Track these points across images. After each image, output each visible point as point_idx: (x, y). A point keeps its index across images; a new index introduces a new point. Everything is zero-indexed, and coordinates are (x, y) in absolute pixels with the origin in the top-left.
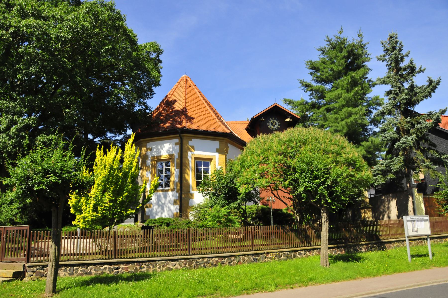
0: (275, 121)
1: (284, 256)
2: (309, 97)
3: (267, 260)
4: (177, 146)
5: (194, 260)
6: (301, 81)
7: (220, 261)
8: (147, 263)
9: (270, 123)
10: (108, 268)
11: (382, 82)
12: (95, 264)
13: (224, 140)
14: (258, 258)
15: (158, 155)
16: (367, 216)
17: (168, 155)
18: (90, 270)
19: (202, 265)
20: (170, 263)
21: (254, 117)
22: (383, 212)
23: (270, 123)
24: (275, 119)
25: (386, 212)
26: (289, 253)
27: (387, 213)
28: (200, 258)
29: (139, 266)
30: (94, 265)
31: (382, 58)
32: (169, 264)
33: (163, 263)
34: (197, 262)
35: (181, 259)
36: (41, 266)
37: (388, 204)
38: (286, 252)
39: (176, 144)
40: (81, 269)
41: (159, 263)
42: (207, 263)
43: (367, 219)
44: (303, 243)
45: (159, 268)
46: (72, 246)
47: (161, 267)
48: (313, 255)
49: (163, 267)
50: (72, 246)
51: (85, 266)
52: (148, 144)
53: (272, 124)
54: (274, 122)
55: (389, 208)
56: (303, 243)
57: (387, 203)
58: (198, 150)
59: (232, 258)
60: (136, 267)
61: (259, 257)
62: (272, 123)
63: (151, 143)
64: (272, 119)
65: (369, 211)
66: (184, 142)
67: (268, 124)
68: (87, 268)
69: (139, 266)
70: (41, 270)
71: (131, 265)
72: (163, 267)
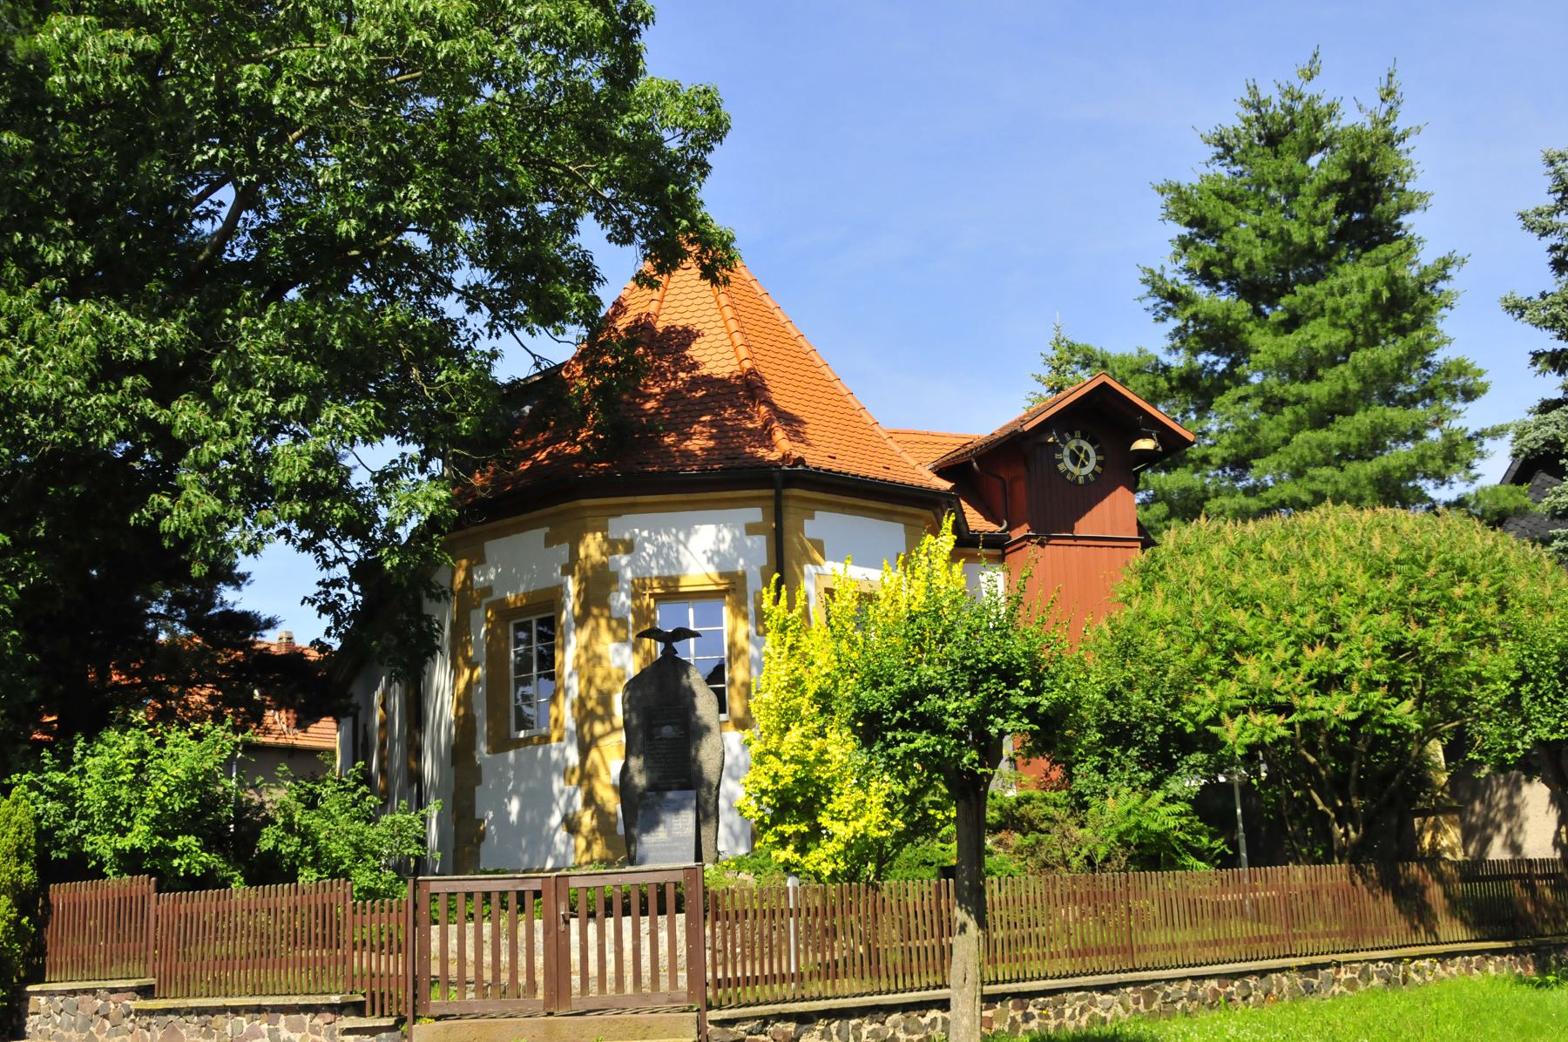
0: (1086, 446)
1: (1380, 974)
2: (1169, 343)
3: (1336, 989)
4: (756, 538)
5: (1158, 988)
6: (1152, 272)
7: (1221, 990)
8: (1041, 1000)
9: (1066, 452)
10: (940, 1021)
11: (1545, 320)
12: (905, 1008)
13: (918, 517)
14: (1316, 982)
15: (666, 573)
16: (1445, 843)
17: (715, 577)
18: (891, 1032)
19: (1179, 1006)
20: (1098, 996)
21: (1027, 428)
22: (1484, 827)
23: (1066, 452)
24: (1083, 438)
25: (1498, 828)
26: (1391, 966)
27: (1504, 830)
28: (1173, 980)
29: (1020, 1012)
30: (903, 1012)
31: (1545, 220)
32: (1093, 1003)
33: (1079, 998)
34: (1167, 995)
35: (1125, 985)
36: (760, 1017)
37: (1510, 797)
38: (1385, 960)
39: (751, 529)
40: (870, 1028)
41: (1070, 997)
42: (1192, 997)
43: (1448, 855)
44: (1416, 929)
45: (1072, 1017)
46: (610, 957)
47: (1077, 1012)
48: (1451, 974)
49: (1081, 1014)
50: (610, 957)
51: (881, 1014)
52: (612, 522)
53: (1075, 459)
54: (1080, 449)
55: (1512, 811)
56: (1416, 929)
57: (1503, 792)
58: (839, 558)
59: (1252, 982)
60: (1012, 1013)
61: (1317, 978)
62: (1072, 452)
63: (627, 519)
64: (1073, 436)
65: (1453, 823)
66: (789, 521)
67: (1057, 456)
68: (883, 1023)
69: (1020, 1012)
70: (761, 1033)
71: (998, 1006)
72: (1081, 1014)
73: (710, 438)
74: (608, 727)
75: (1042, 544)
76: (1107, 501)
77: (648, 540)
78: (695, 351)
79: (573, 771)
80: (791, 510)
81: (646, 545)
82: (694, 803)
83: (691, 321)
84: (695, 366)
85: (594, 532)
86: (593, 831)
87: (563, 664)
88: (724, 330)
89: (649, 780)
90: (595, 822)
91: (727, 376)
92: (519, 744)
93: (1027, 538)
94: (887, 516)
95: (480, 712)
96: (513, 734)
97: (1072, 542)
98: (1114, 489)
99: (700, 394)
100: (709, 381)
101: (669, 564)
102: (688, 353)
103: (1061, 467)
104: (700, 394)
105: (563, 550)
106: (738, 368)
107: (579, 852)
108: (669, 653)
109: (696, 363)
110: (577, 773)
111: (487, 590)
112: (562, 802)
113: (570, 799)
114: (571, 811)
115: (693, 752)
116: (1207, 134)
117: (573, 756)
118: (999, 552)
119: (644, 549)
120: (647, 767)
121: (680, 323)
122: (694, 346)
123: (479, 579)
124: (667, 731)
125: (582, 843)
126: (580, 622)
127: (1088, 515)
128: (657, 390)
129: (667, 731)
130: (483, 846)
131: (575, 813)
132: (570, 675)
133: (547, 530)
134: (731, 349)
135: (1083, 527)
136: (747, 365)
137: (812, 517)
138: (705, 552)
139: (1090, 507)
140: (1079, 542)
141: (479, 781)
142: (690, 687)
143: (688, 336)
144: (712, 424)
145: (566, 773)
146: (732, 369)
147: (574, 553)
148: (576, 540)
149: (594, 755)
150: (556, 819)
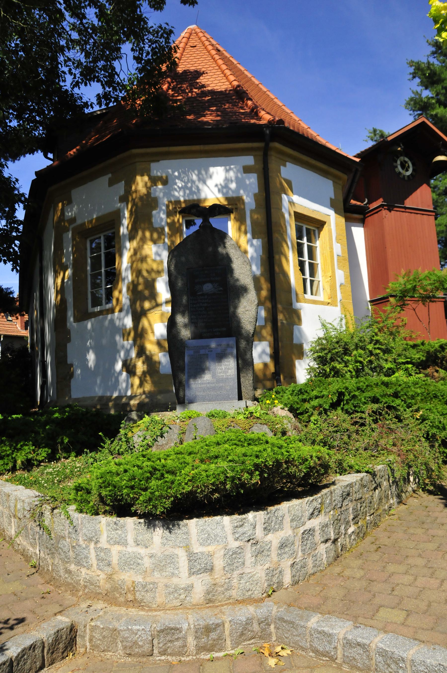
4: (251, 175)
9: (399, 162)
23: (399, 162)
39: (247, 170)
52: (153, 165)
53: (403, 165)
63: (164, 163)
73: (218, 116)
74: (154, 303)
75: (390, 211)
76: (418, 191)
77: (179, 178)
78: (202, 80)
79: (129, 334)
80: (273, 158)
81: (177, 181)
82: (235, 352)
83: (198, 67)
84: (203, 86)
85: (142, 175)
86: (144, 373)
87: (121, 263)
88: (219, 70)
89: (192, 333)
90: (145, 367)
91: (224, 90)
92: (95, 315)
93: (382, 206)
94: (324, 174)
95: (70, 300)
96: (90, 310)
97: (403, 210)
98: (421, 185)
99: (207, 98)
100: (213, 93)
101: (192, 193)
102: (198, 81)
103: (397, 170)
104: (207, 98)
105: (120, 188)
106: (230, 86)
107: (135, 387)
108: (206, 226)
109: (204, 85)
110: (132, 334)
111: (73, 220)
112: (122, 354)
113: (128, 352)
114: (129, 358)
115: (232, 309)
116: (430, 41)
117: (128, 322)
118: (361, 216)
119: (176, 184)
120: (193, 322)
121: (192, 68)
122: (201, 78)
123: (69, 214)
124: (208, 287)
125: (136, 381)
126: (131, 238)
127: (410, 197)
128: (180, 98)
129: (208, 287)
130: (72, 381)
131: (131, 359)
132: (126, 269)
133: (110, 175)
134: (224, 78)
135: (409, 203)
136: (235, 83)
137: (285, 166)
138: (216, 185)
139: (411, 194)
140: (407, 210)
141: (69, 340)
142: (227, 254)
143: (198, 74)
144: (217, 110)
145: (125, 334)
146: (226, 87)
147: (128, 191)
148: (130, 181)
149: (144, 322)
150: (119, 366)
